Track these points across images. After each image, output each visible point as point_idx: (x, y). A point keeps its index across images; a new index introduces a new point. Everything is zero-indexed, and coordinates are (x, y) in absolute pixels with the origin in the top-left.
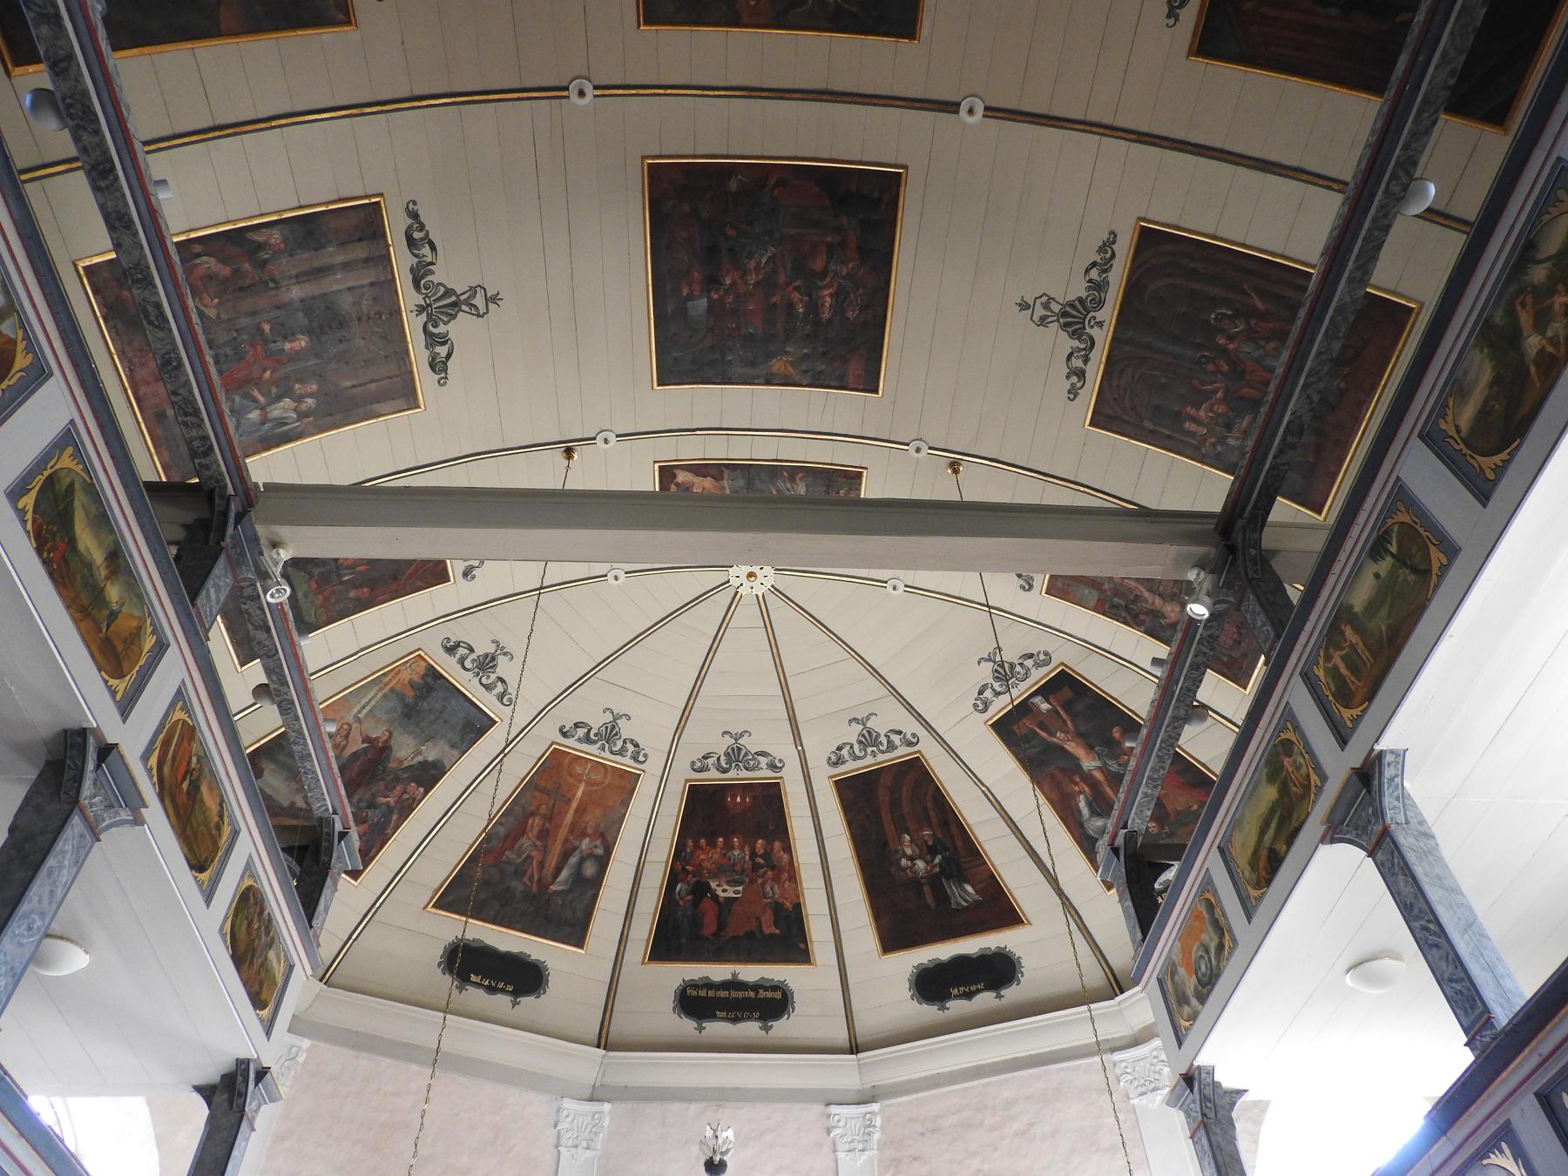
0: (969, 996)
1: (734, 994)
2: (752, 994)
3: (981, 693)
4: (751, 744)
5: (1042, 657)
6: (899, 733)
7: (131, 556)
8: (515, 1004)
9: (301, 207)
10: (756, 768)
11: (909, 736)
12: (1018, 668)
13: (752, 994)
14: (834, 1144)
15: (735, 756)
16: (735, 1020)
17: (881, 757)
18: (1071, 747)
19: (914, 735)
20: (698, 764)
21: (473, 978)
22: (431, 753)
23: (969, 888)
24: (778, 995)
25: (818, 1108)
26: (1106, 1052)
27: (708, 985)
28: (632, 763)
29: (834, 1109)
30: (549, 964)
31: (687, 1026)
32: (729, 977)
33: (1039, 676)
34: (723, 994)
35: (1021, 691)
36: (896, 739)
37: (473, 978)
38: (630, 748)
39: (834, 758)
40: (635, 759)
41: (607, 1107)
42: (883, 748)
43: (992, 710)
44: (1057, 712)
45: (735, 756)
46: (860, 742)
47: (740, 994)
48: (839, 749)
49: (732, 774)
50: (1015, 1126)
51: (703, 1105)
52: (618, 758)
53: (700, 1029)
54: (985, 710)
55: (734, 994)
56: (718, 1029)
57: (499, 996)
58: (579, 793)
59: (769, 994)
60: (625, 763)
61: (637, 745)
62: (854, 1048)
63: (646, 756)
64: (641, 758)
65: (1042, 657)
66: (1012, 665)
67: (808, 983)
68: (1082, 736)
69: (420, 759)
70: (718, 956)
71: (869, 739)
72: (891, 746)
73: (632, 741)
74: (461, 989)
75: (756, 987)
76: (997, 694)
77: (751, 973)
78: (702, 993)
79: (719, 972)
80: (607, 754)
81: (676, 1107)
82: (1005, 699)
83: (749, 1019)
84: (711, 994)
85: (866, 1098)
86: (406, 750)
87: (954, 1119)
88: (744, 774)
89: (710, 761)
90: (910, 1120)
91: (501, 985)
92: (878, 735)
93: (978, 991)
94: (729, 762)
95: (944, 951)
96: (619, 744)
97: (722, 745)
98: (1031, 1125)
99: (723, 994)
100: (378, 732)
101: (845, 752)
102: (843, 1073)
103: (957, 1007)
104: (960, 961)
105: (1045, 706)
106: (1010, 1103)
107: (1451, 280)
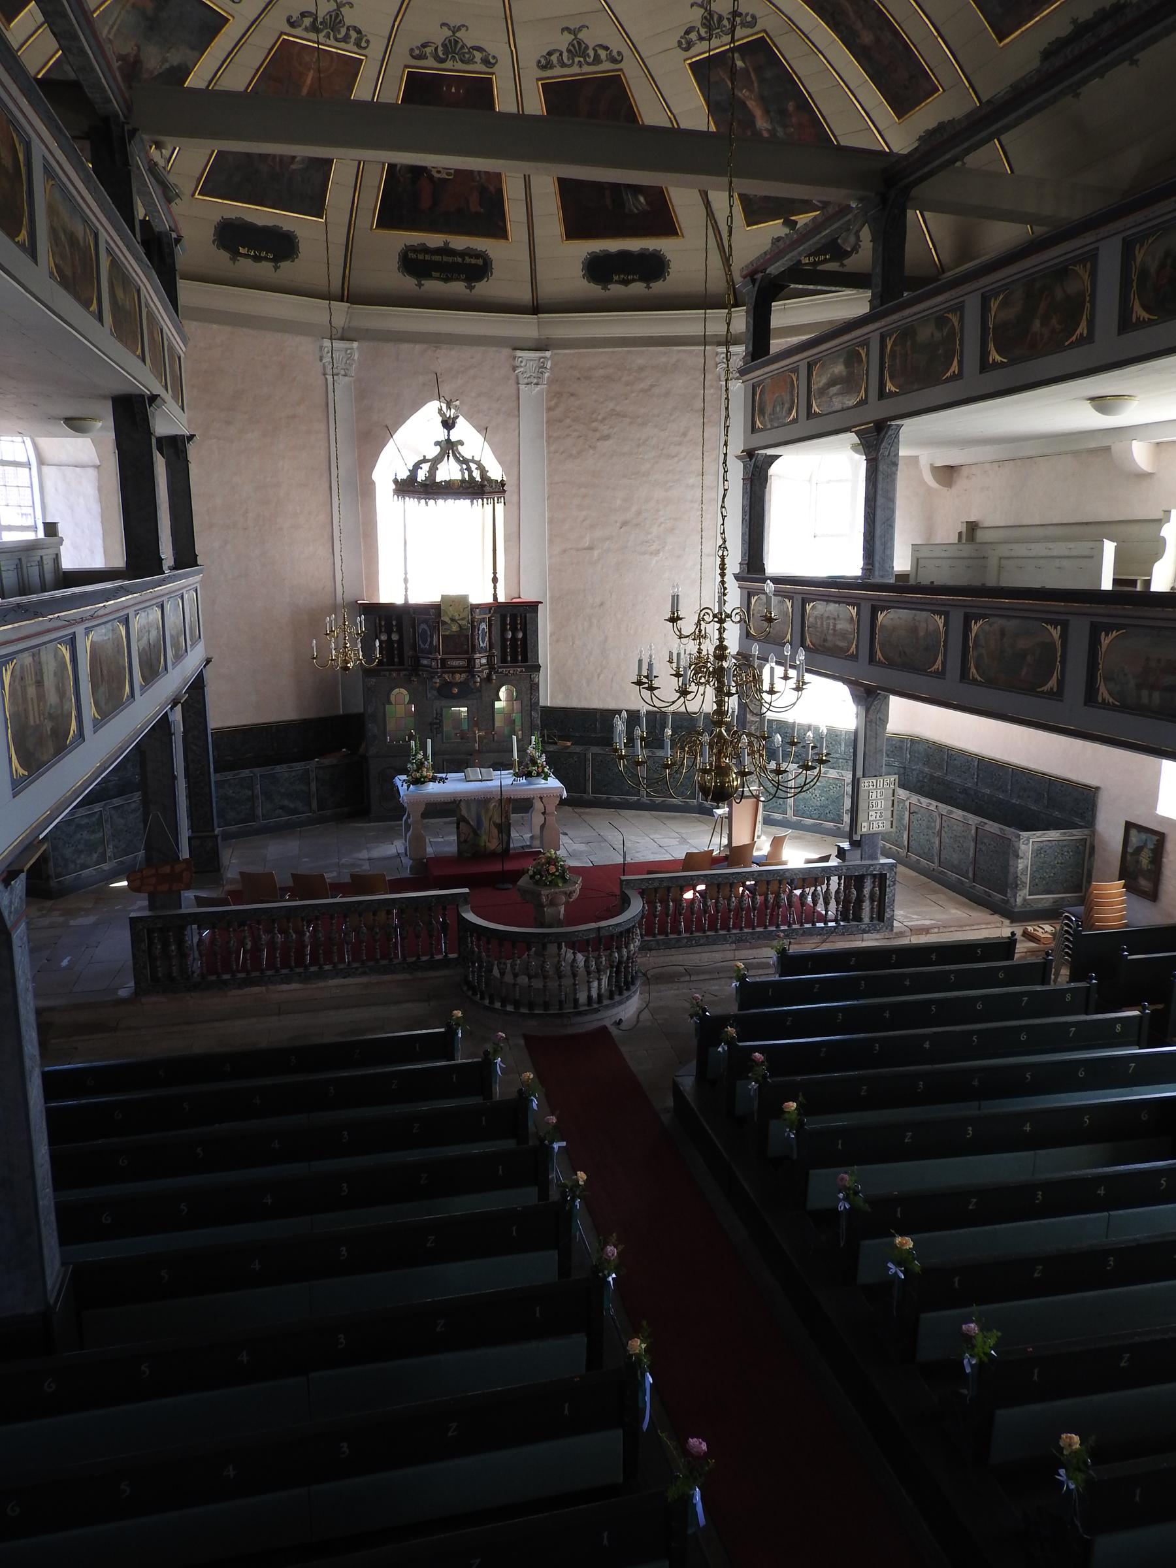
0: (626, 283)
1: (446, 259)
2: (460, 260)
3: (687, 32)
4: (468, 38)
5: (749, 19)
6: (606, 48)
7: (101, 206)
8: (276, 268)
9: (258, 70)
10: (471, 61)
11: (615, 53)
12: (725, 22)
13: (460, 260)
14: (517, 377)
15: (452, 48)
16: (446, 280)
17: (586, 69)
18: (751, 104)
19: (619, 53)
20: (417, 52)
21: (241, 250)
22: (175, 58)
23: (642, 199)
24: (480, 262)
25: (506, 352)
26: (711, 344)
27: (424, 249)
28: (355, 49)
29: (519, 353)
30: (298, 233)
31: (408, 283)
32: (442, 245)
33: (744, 35)
34: (437, 258)
35: (720, 44)
36: (603, 54)
37: (241, 250)
38: (353, 35)
39: (543, 62)
40: (358, 45)
41: (355, 345)
42: (590, 60)
43: (693, 51)
44: (748, 71)
45: (452, 48)
46: (569, 51)
47: (450, 259)
48: (550, 54)
49: (449, 64)
50: (643, 385)
51: (425, 346)
52: (342, 45)
53: (420, 285)
54: (687, 49)
55: (446, 259)
56: (433, 286)
57: (264, 264)
58: (309, 81)
59: (473, 261)
60: (348, 51)
61: (359, 32)
62: (535, 309)
63: (368, 42)
64: (364, 44)
65: (749, 19)
66: (720, 18)
67: (506, 254)
68: (762, 99)
69: (167, 65)
70: (433, 228)
71: (578, 49)
72: (597, 60)
73: (355, 28)
74: (234, 259)
75: (463, 254)
76: (701, 39)
77: (459, 242)
78: (421, 257)
79: (434, 240)
80: (332, 42)
81: (406, 347)
82: (704, 45)
83: (457, 279)
84: (427, 257)
85: (540, 346)
86: (154, 60)
87: (601, 372)
88: (460, 65)
89: (428, 50)
90: (571, 367)
91: (263, 254)
92: (587, 47)
93: (634, 280)
94: (446, 53)
95: (613, 245)
96: (343, 31)
97: (439, 36)
98: (652, 386)
99: (437, 258)
100: (128, 48)
101: (554, 58)
102: (526, 327)
103: (616, 290)
104: (624, 255)
105: (739, 64)
106: (642, 369)
107: (865, 549)
